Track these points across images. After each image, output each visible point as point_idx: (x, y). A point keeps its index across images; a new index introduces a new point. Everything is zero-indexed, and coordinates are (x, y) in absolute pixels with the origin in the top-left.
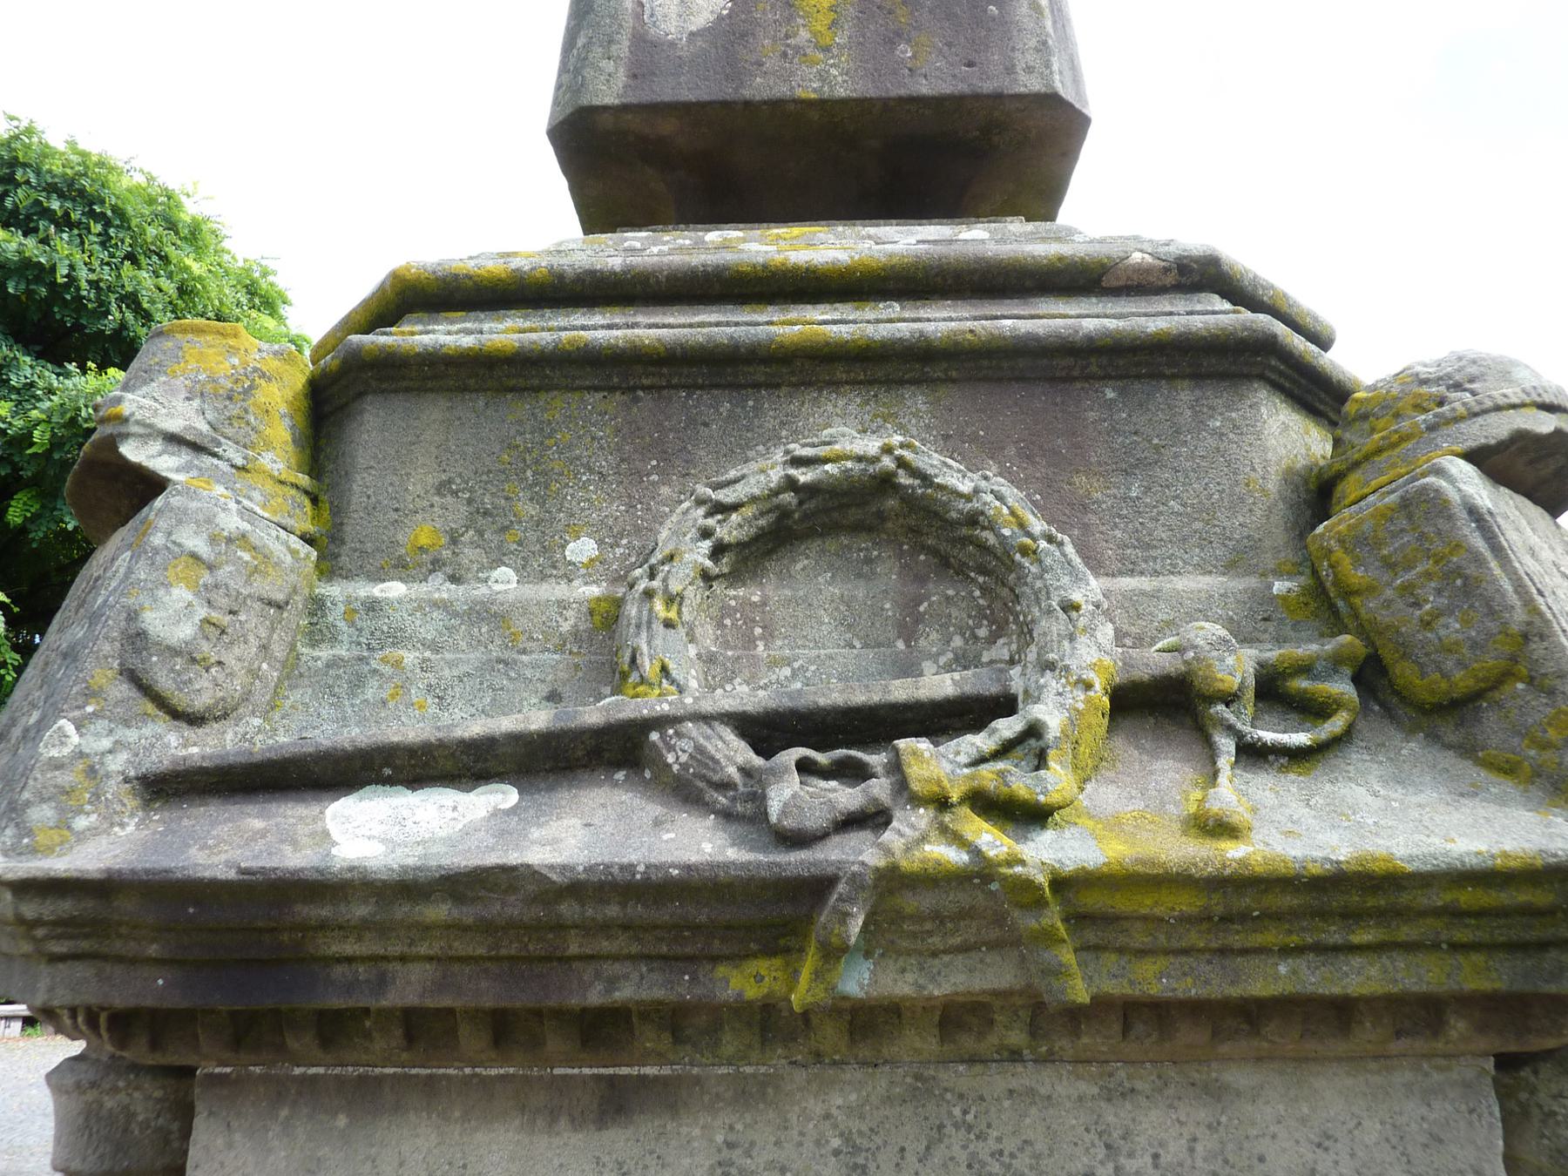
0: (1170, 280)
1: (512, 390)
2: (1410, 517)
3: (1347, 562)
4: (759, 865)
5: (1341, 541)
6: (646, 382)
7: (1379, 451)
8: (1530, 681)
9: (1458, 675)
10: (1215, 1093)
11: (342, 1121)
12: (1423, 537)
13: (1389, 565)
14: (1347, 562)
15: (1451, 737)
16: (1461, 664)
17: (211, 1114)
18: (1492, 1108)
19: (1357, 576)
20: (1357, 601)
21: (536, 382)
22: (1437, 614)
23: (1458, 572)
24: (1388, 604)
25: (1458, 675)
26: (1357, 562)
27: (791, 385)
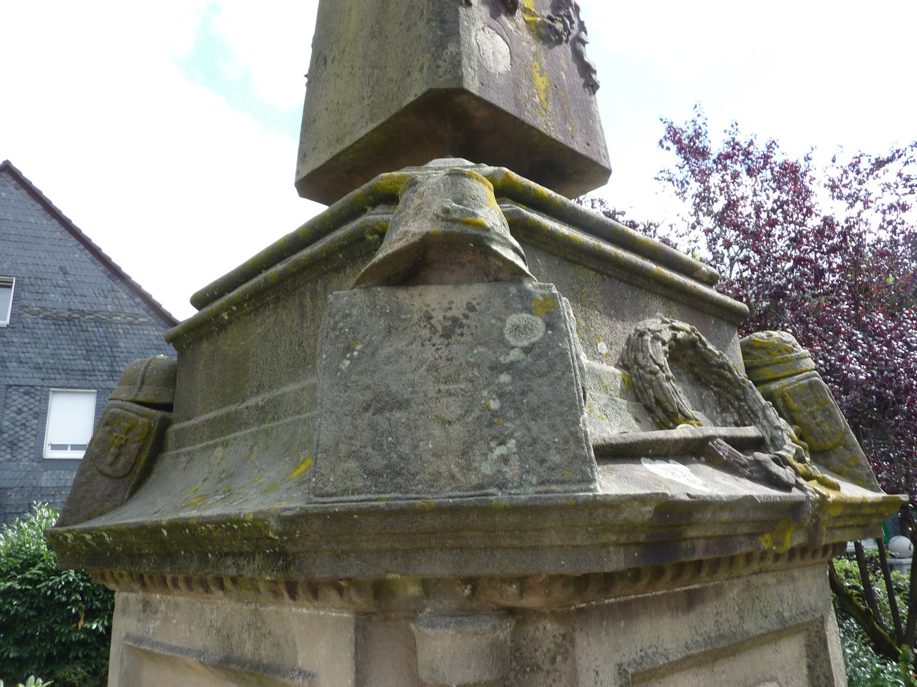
0: (706, 279)
1: (567, 260)
2: (812, 389)
3: (791, 401)
4: (785, 497)
5: (789, 393)
6: (610, 272)
7: (779, 363)
8: (845, 447)
9: (828, 442)
10: (793, 579)
11: (623, 623)
12: (816, 396)
13: (805, 404)
14: (791, 401)
15: (822, 462)
16: (830, 439)
17: (581, 629)
18: (348, 635)
19: (795, 406)
20: (795, 414)
21: (576, 259)
22: (822, 422)
23: (828, 410)
24: (805, 417)
25: (828, 442)
26: (795, 401)
27: (646, 290)
